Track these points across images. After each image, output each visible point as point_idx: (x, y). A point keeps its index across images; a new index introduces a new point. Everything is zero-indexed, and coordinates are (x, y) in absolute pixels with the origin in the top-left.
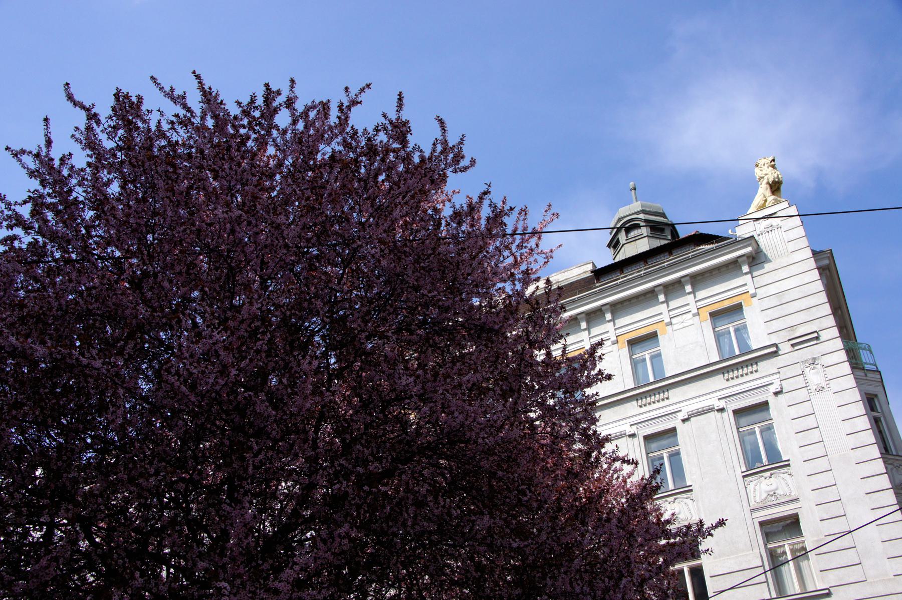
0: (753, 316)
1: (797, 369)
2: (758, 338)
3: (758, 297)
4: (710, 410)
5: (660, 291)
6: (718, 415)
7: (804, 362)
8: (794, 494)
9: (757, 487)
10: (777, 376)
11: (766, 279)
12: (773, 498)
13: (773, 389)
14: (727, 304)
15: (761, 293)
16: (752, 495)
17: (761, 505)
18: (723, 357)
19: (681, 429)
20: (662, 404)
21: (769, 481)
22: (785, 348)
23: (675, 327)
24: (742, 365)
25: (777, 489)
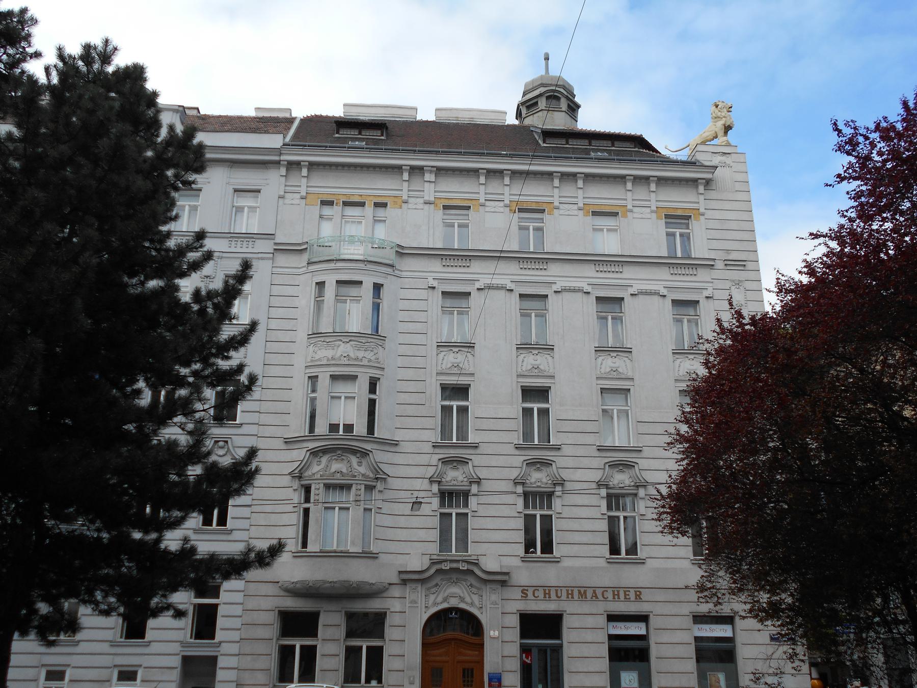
0: (697, 229)
1: (727, 285)
2: (700, 249)
3: (706, 216)
4: (656, 293)
5: (405, 170)
6: (661, 299)
7: (733, 281)
8: (630, 374)
9: (682, 364)
10: (710, 285)
11: (713, 205)
12: (615, 373)
13: (706, 293)
14: (679, 213)
15: (709, 214)
16: (440, 362)
17: (604, 376)
18: (188, 229)
19: (628, 300)
20: (615, 275)
21: (614, 360)
22: (720, 265)
23: (487, 209)
24: (693, 266)
25: (540, 365)
